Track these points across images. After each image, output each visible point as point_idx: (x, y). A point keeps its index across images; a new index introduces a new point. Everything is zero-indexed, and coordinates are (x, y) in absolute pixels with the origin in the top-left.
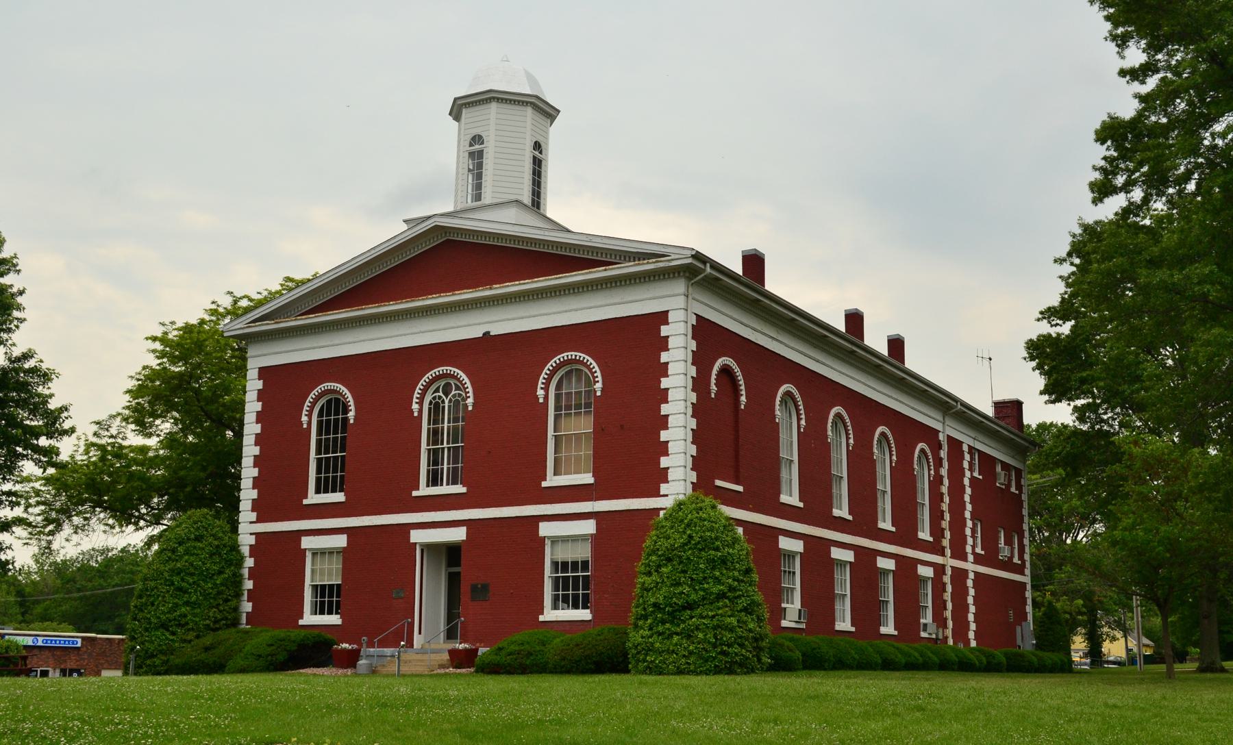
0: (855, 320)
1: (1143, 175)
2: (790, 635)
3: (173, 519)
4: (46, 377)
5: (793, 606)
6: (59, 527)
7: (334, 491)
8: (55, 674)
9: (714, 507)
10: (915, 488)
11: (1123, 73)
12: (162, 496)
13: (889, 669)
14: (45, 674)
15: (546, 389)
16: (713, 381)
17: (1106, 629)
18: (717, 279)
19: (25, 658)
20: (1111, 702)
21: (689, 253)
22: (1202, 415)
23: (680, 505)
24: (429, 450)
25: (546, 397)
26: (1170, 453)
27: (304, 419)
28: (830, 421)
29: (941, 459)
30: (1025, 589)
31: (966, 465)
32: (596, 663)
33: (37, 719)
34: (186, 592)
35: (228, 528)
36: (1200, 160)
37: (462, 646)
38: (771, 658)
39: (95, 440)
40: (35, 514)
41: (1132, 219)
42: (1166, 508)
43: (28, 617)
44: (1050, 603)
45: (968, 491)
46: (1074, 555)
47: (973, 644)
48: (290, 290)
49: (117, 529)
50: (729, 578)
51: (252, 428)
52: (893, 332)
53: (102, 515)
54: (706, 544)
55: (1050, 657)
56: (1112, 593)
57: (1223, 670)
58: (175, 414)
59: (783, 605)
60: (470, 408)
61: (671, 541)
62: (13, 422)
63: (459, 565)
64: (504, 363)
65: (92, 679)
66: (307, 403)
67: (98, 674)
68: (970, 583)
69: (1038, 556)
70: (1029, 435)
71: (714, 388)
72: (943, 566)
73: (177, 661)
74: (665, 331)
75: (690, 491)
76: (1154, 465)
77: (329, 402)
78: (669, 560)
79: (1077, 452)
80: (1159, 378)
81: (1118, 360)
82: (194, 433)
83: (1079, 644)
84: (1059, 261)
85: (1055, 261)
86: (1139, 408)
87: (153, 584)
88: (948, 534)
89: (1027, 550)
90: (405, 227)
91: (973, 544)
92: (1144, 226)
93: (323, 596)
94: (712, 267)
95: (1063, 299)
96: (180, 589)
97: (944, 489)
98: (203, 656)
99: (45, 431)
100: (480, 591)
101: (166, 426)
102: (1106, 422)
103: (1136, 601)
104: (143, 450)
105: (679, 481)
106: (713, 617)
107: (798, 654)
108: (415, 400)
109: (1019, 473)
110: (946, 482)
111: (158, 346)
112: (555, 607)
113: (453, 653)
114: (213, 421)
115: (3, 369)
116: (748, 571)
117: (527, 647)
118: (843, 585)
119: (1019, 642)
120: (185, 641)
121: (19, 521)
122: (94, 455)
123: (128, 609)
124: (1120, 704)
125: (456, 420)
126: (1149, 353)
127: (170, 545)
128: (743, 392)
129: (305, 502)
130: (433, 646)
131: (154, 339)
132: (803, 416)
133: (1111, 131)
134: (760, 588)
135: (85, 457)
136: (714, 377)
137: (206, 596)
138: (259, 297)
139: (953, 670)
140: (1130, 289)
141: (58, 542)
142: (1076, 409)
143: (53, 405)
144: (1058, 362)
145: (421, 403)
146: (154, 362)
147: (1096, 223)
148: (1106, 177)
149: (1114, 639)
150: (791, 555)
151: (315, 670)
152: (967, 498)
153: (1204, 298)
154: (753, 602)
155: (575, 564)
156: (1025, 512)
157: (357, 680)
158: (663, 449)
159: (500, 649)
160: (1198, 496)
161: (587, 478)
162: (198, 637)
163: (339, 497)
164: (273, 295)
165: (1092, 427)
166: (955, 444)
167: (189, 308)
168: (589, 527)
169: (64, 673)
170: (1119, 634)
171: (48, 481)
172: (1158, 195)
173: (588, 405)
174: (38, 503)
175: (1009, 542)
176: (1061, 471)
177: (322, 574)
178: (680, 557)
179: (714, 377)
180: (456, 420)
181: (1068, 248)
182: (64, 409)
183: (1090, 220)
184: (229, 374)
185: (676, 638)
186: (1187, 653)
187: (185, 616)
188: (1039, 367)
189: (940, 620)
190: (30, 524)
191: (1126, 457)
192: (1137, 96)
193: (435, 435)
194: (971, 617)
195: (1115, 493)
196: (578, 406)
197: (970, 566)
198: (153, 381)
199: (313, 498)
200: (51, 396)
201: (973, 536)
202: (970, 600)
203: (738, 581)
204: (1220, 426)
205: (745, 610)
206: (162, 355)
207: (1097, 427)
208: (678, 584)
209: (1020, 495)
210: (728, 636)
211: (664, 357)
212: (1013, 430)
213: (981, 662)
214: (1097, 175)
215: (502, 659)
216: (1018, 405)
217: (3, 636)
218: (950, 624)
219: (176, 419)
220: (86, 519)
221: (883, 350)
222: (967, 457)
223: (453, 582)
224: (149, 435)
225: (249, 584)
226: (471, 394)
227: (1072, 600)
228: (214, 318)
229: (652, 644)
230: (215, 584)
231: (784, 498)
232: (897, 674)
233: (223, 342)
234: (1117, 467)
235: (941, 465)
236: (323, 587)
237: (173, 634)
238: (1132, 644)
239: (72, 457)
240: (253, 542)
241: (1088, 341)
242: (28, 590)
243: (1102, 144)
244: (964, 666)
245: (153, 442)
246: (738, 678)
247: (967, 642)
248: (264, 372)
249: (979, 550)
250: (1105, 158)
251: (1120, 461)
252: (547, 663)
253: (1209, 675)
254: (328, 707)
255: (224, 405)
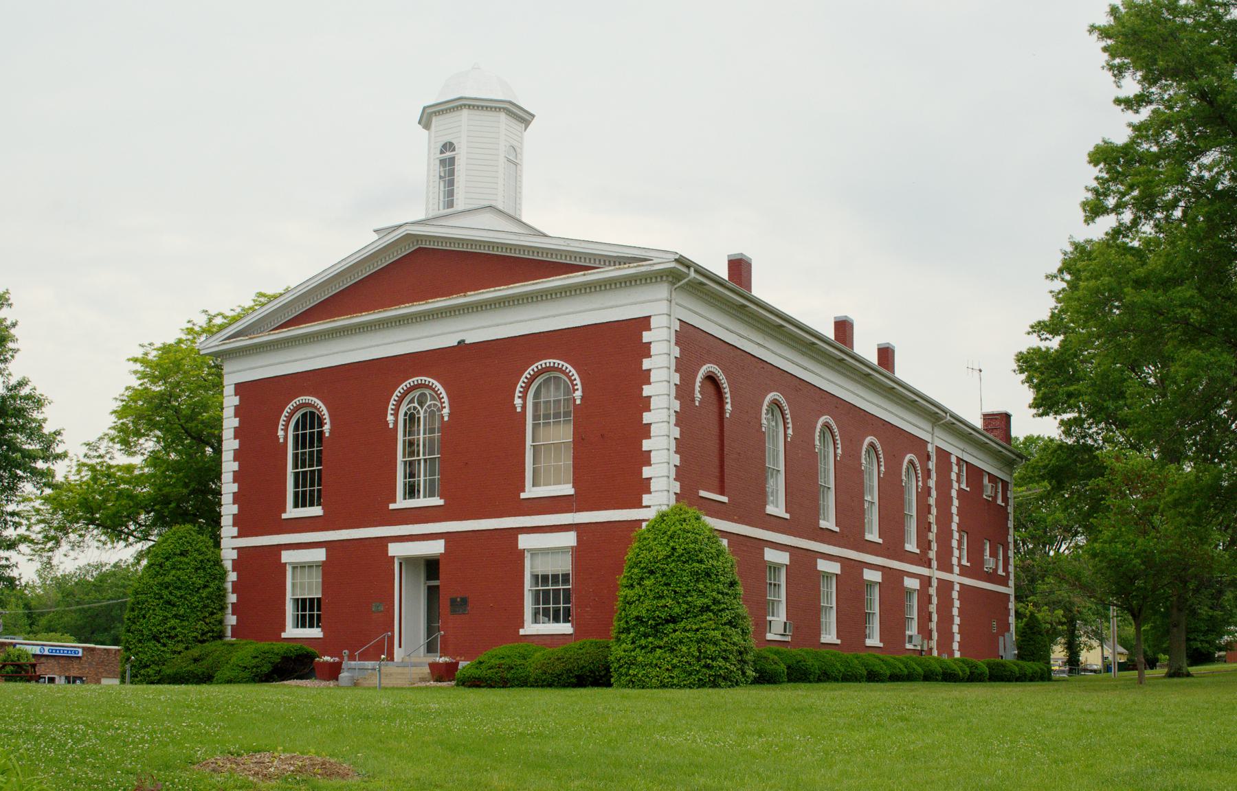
0: (844, 328)
1: (1134, 198)
2: (775, 647)
3: (160, 535)
4: (39, 403)
5: (779, 619)
6: (58, 543)
7: (312, 505)
8: (60, 681)
9: (698, 518)
10: (902, 499)
11: (1118, 101)
12: (148, 513)
13: (873, 681)
14: (52, 680)
15: (524, 398)
16: (697, 389)
17: (1083, 639)
18: (702, 284)
19: (34, 666)
20: (1086, 708)
21: (673, 257)
22: (1179, 434)
23: (662, 517)
24: (405, 462)
25: (524, 407)
26: (1150, 467)
27: (281, 433)
28: (818, 430)
29: (929, 471)
30: (1008, 600)
31: (954, 476)
32: (577, 677)
33: (47, 722)
34: (174, 605)
35: (211, 543)
36: (1187, 189)
37: (442, 660)
38: (756, 671)
39: (86, 461)
40: (36, 532)
41: (1121, 240)
42: (1143, 521)
43: (35, 628)
44: (1032, 614)
45: (956, 502)
46: (1056, 569)
47: (957, 655)
48: (263, 305)
49: (109, 545)
50: (713, 590)
51: (230, 445)
52: (883, 341)
53: (95, 532)
54: (690, 557)
55: (1030, 666)
56: (1090, 604)
57: (1188, 675)
58: (158, 433)
59: (769, 618)
60: (446, 419)
61: (654, 553)
62: (13, 447)
63: (438, 578)
64: (481, 374)
65: (93, 686)
66: (283, 418)
67: (98, 682)
68: (955, 595)
69: (1023, 569)
70: (1017, 447)
71: (698, 395)
72: (930, 578)
73: (169, 671)
74: (647, 337)
75: (673, 502)
76: (1134, 479)
77: (304, 415)
78: (652, 572)
79: (1065, 467)
80: (1141, 395)
81: (1105, 376)
82: (176, 451)
83: (1058, 654)
84: (1051, 277)
85: (1047, 277)
86: (1122, 424)
87: (143, 597)
88: (934, 546)
89: (1012, 561)
90: (375, 237)
91: (959, 556)
92: (1132, 248)
93: (304, 609)
94: (696, 271)
95: (1053, 314)
96: (169, 602)
97: (932, 501)
98: (192, 667)
99: (41, 454)
100: (459, 605)
101: (149, 444)
102: (1091, 436)
103: (1113, 611)
104: (129, 468)
105: (661, 492)
106: (697, 630)
107: (783, 667)
108: (390, 412)
109: (1005, 484)
110: (934, 493)
111: (138, 367)
112: (536, 621)
113: (433, 666)
114: (193, 438)
115: (3, 397)
116: (732, 584)
117: (507, 661)
118: (830, 598)
119: (1001, 652)
120: (175, 652)
121: (24, 539)
122: (86, 475)
123: (122, 622)
124: (1094, 710)
125: (432, 431)
126: (1133, 370)
127: (159, 562)
128: (729, 400)
129: (284, 516)
130: (414, 660)
131: (136, 360)
132: (790, 425)
133: (1104, 155)
134: (746, 601)
135: (77, 477)
136: (698, 384)
137: (194, 609)
138: (233, 313)
139: (937, 680)
140: (1118, 308)
141: (57, 557)
142: (1062, 423)
143: (47, 429)
144: (1050, 377)
145: (396, 415)
146: (135, 383)
147: (1087, 241)
148: (1098, 199)
149: (1091, 648)
150: (775, 568)
151: (299, 682)
152: (954, 510)
153: (1185, 321)
154: (738, 615)
155: (555, 577)
156: (1011, 524)
157: (339, 692)
158: (646, 459)
159: (481, 663)
160: (1172, 511)
161: (568, 489)
162: (187, 648)
163: (317, 511)
164: (246, 312)
165: (1078, 442)
166: (943, 455)
167: (166, 329)
168: (570, 539)
169: (68, 680)
170: (1095, 643)
171: (47, 500)
172: (1146, 218)
173: (567, 414)
174: (39, 522)
175: (994, 554)
176: (1046, 483)
177: (302, 588)
178: (663, 570)
179: (698, 384)
180: (432, 431)
181: (1059, 265)
182: (58, 433)
183: (1080, 239)
184: (206, 391)
185: (659, 651)
186: (1157, 660)
187: (175, 628)
188: (1029, 380)
189: (925, 633)
190: (32, 541)
191: (1108, 471)
192: (1130, 125)
193: (411, 445)
194: (955, 629)
195: (1097, 506)
196: (557, 415)
197: (956, 578)
198: (136, 402)
199: (291, 512)
200: (45, 420)
201: (959, 548)
202: (955, 612)
203: (722, 593)
204: (1195, 444)
205: (730, 623)
206: (144, 376)
207: (1082, 441)
208: (661, 597)
209: (1005, 508)
210: (711, 649)
211: (646, 364)
212: (1004, 444)
213: (963, 671)
214: (1090, 196)
215: (482, 672)
216: (1006, 417)
217: (3, 644)
218: (935, 635)
219: (158, 437)
220: (80, 536)
221: (873, 358)
222: (955, 469)
223: (432, 593)
224: (133, 454)
225: (232, 598)
226: (446, 405)
227: (1052, 610)
228: (190, 337)
229: (635, 658)
230: (201, 598)
231: (770, 509)
232: (881, 685)
233: (199, 360)
234: (1100, 480)
235: (929, 477)
236: (304, 600)
237: (164, 645)
238: (1108, 652)
239: (66, 478)
240: (235, 557)
241: (1076, 356)
242: (33, 603)
243: (1096, 165)
244: (949, 677)
245: (137, 460)
246: (722, 691)
247: (951, 653)
248: (240, 388)
249: (964, 562)
250: (1097, 178)
251: (1103, 475)
252: (528, 677)
253: (1175, 680)
254: (312, 718)
255: (203, 422)
